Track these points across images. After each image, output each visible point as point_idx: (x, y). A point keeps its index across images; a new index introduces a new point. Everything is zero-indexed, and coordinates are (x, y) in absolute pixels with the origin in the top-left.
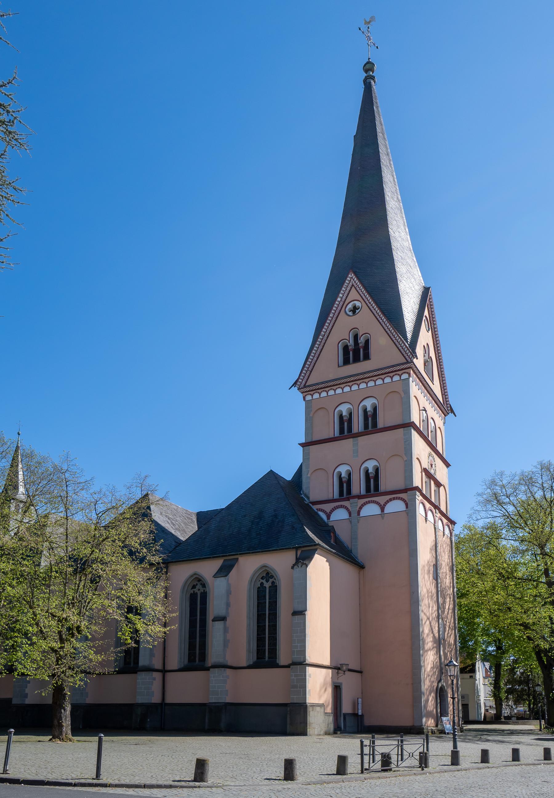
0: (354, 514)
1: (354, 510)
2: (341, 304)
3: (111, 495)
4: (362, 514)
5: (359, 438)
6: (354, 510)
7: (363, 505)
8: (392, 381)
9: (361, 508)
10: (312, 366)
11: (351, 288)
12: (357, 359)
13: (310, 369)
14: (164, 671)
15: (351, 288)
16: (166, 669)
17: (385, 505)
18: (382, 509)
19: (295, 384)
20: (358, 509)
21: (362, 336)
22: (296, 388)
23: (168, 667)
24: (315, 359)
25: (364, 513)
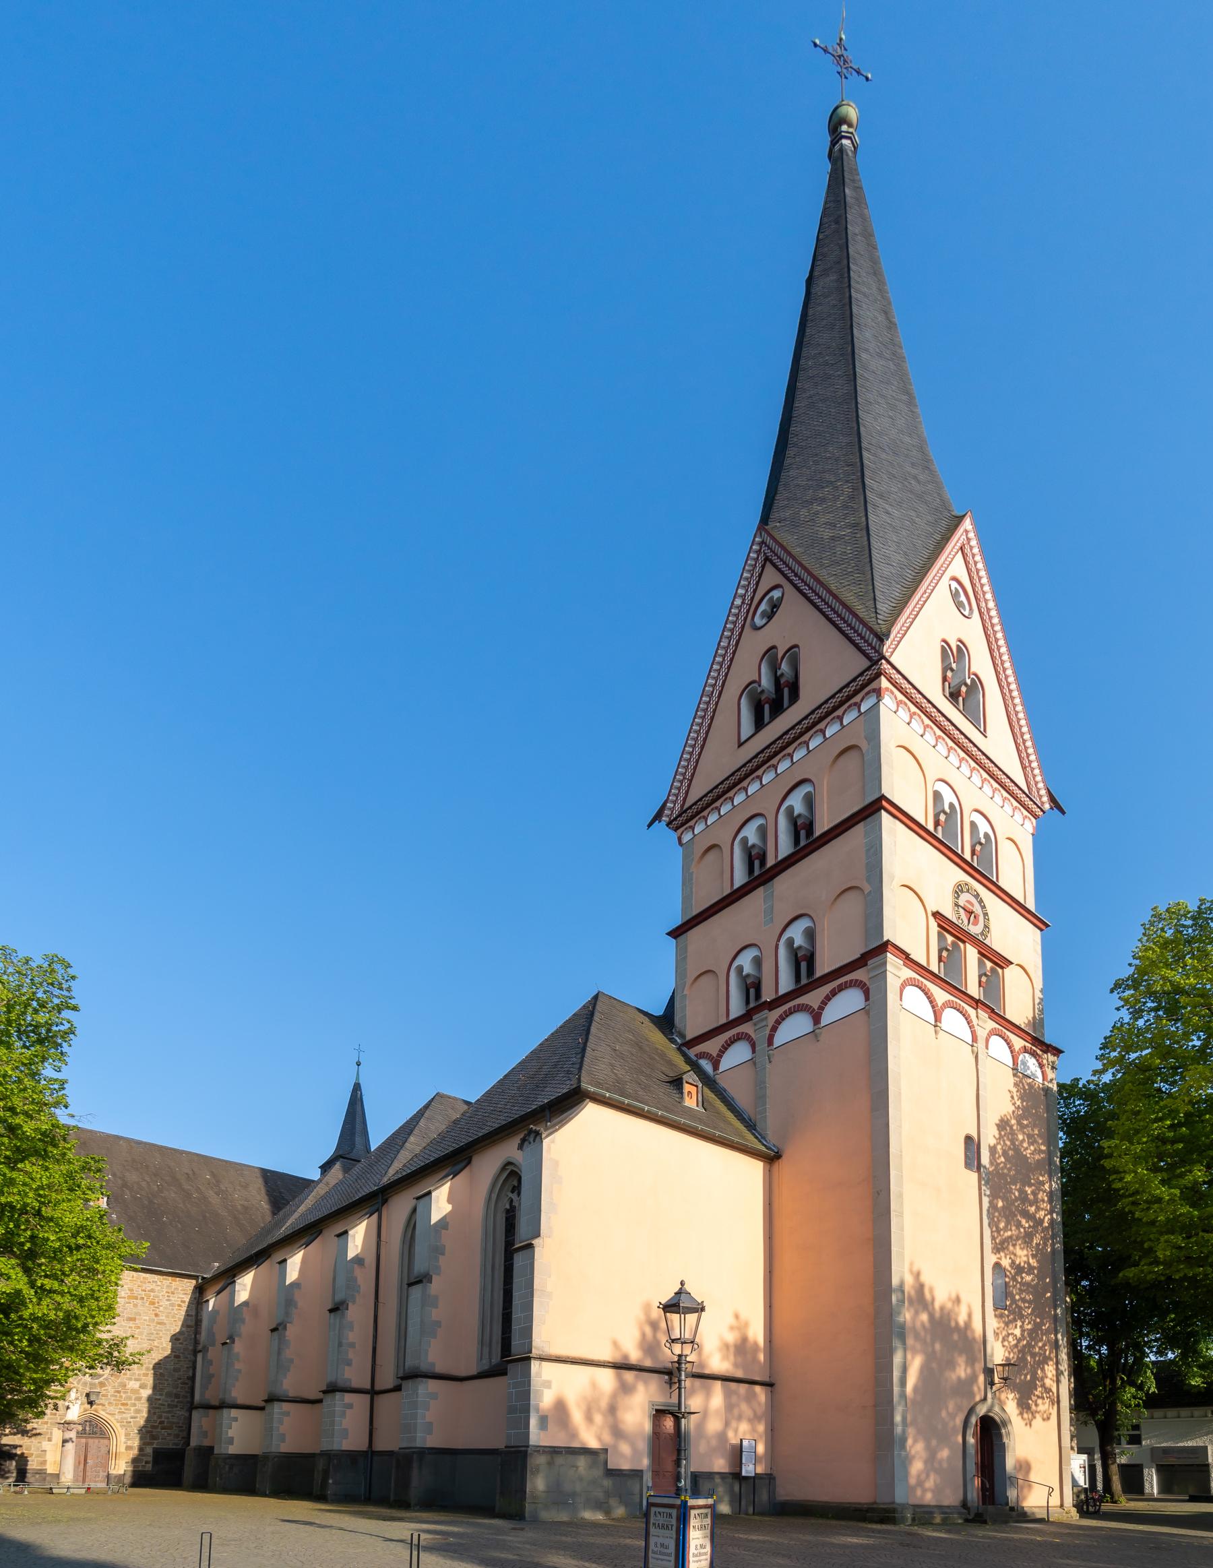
0: (762, 1046)
1: (760, 1037)
2: (744, 610)
3: (83, 1291)
4: (779, 1040)
5: (689, 933)
6: (760, 1037)
7: (778, 1022)
8: (826, 739)
9: (774, 1029)
10: (691, 767)
11: (763, 567)
12: (778, 708)
13: (688, 775)
14: (373, 1393)
15: (763, 567)
16: (368, 1397)
17: (822, 1008)
18: (817, 1018)
19: (658, 817)
20: (768, 1032)
21: (783, 658)
22: (663, 824)
23: (361, 1401)
24: (697, 750)
25: (781, 1037)
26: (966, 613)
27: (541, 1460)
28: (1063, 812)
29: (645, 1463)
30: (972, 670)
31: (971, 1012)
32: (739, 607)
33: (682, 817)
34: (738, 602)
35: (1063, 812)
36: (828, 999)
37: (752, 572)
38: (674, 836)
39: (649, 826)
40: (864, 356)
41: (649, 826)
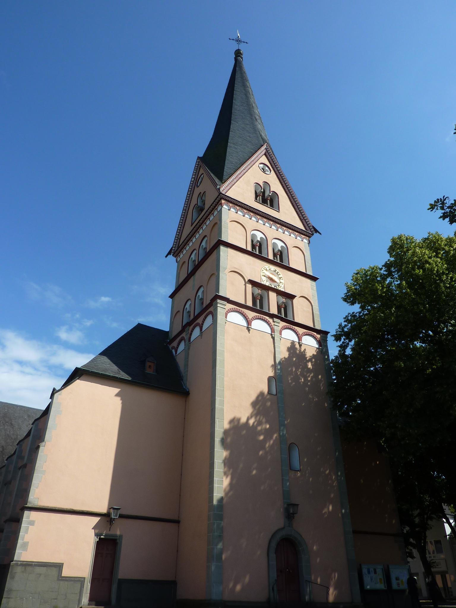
1: (186, 338)
2: (195, 182)
4: (192, 339)
17: (203, 324)
19: (169, 253)
26: (269, 173)
27: (19, 570)
28: (320, 234)
29: (407, 587)
30: (272, 190)
31: (271, 320)
32: (193, 181)
33: (175, 251)
34: (193, 180)
35: (320, 234)
36: (204, 320)
37: (196, 170)
38: (175, 259)
39: (166, 257)
40: (236, 107)
41: (166, 257)
